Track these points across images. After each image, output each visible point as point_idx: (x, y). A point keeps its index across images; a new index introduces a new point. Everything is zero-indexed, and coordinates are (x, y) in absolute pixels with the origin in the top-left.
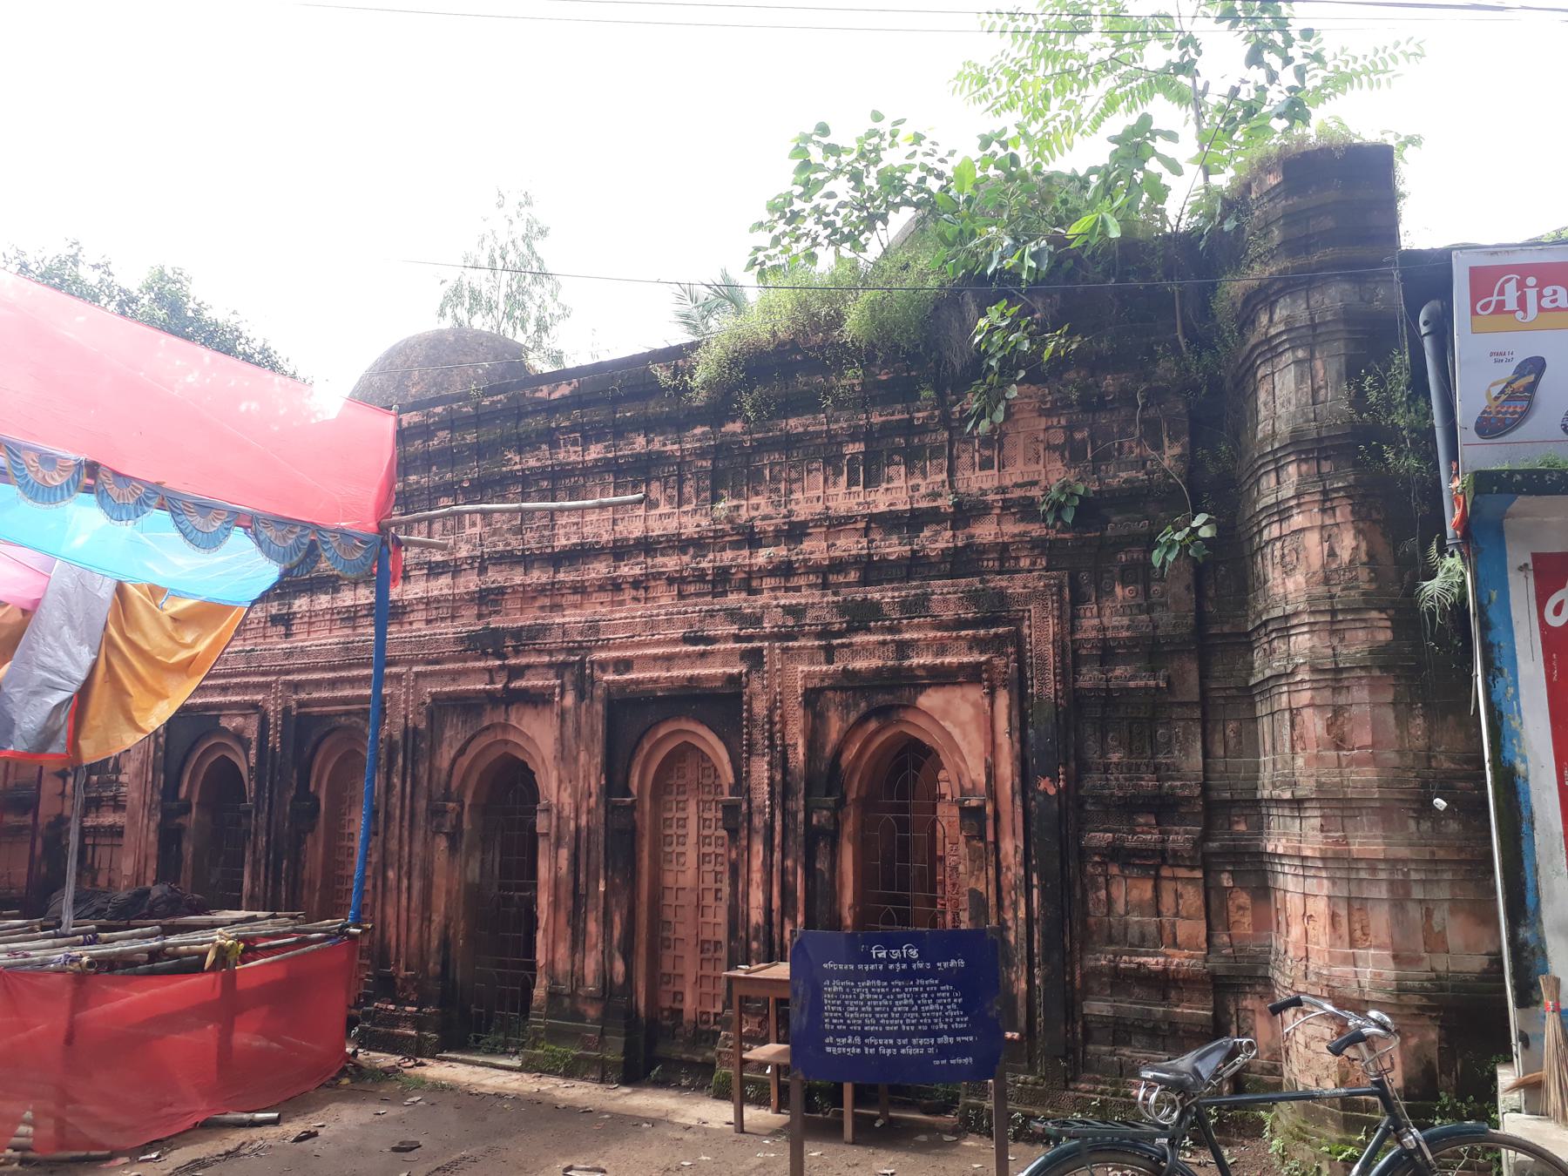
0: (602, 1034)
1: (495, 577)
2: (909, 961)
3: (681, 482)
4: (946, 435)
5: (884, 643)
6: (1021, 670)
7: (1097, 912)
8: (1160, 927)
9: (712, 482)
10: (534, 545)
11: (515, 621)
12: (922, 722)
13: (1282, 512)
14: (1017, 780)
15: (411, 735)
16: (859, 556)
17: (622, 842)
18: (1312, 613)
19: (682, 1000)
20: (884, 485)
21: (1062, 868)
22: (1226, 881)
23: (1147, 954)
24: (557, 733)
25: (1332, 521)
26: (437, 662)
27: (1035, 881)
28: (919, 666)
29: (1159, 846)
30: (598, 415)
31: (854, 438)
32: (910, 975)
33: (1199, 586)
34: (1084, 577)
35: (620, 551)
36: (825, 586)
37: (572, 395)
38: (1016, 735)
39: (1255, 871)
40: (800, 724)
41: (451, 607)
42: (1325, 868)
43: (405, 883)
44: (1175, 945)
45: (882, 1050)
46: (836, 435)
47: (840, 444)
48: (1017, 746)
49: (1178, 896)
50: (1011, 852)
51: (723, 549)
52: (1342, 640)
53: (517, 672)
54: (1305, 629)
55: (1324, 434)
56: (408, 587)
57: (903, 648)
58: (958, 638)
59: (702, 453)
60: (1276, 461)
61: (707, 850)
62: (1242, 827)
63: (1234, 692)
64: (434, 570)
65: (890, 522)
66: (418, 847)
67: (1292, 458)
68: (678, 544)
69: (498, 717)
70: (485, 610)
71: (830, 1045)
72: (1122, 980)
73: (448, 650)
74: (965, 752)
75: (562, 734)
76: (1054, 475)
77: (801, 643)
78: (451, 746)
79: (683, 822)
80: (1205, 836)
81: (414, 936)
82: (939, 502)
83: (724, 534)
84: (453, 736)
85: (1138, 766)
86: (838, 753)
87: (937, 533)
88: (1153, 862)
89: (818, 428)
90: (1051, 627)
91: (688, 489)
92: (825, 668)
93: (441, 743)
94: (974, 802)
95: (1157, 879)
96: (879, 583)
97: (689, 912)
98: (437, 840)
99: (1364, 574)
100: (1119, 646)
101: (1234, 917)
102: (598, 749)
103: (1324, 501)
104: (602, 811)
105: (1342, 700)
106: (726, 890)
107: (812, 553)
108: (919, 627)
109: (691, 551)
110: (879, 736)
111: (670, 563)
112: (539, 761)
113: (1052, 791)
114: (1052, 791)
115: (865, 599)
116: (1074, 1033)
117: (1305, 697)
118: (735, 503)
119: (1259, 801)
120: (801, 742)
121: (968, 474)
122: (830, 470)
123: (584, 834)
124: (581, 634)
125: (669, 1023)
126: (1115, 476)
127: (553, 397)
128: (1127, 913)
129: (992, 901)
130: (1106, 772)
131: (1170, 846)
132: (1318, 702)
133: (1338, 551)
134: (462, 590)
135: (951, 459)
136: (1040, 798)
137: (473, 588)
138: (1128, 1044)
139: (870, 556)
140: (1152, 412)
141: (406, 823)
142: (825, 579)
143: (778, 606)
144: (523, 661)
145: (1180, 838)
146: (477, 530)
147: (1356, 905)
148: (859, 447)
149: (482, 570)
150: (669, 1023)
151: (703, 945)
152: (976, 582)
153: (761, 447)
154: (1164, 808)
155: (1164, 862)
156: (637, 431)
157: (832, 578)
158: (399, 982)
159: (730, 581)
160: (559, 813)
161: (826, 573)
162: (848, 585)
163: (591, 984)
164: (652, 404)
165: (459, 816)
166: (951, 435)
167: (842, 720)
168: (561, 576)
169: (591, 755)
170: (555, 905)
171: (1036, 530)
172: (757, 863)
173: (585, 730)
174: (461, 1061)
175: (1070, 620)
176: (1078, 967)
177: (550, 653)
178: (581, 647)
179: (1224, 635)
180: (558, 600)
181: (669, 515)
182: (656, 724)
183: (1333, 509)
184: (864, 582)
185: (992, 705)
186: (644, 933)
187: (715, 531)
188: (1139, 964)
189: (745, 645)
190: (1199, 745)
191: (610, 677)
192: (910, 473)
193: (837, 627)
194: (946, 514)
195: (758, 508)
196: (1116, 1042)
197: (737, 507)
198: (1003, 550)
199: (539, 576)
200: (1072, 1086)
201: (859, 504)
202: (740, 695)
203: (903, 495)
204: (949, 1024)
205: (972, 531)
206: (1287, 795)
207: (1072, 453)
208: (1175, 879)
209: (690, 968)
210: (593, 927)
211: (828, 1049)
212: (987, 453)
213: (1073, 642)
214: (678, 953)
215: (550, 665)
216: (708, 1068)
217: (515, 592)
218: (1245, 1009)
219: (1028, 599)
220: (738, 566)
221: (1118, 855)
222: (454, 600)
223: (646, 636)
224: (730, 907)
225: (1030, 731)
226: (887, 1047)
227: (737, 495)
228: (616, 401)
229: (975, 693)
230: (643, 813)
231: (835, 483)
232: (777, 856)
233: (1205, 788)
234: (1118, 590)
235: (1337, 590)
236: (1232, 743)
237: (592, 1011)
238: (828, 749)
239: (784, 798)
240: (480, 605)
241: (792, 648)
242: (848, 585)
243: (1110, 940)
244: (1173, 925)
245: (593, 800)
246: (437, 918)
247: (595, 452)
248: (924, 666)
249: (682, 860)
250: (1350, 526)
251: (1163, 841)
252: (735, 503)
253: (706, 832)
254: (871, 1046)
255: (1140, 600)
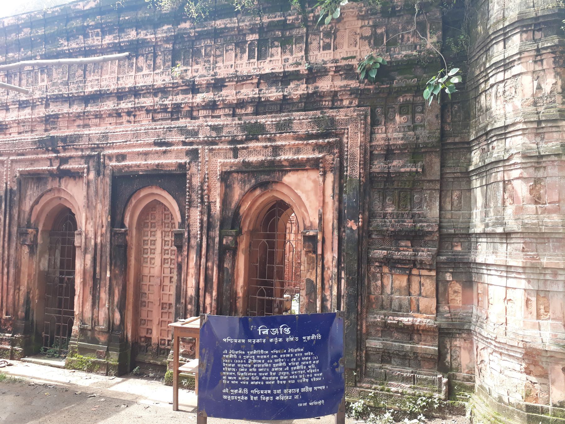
0: (108, 350)
1: (54, 109)
2: (284, 336)
3: (155, 56)
4: (305, 30)
5: (266, 147)
6: (341, 163)
7: (375, 292)
8: (410, 301)
9: (172, 58)
10: (74, 91)
11: (64, 132)
12: (285, 190)
13: (506, 65)
14: (336, 221)
15: (9, 193)
16: (254, 98)
17: (119, 251)
18: (525, 122)
19: (151, 333)
20: (269, 59)
21: (358, 269)
22: (449, 277)
23: (403, 316)
24: (85, 193)
25: (540, 68)
26: (23, 154)
27: (343, 275)
28: (285, 160)
29: (413, 258)
30: (110, 19)
31: (252, 31)
32: (283, 346)
33: (442, 116)
34: (379, 110)
35: (120, 95)
36: (234, 115)
37: (96, 7)
38: (337, 197)
39: (466, 272)
40: (218, 191)
41: (31, 125)
42: (524, 273)
43: (6, 270)
44: (418, 311)
45: (263, 398)
46: (242, 30)
47: (245, 35)
48: (337, 203)
49: (421, 284)
50: (330, 260)
51: (177, 94)
52: (542, 139)
53: (64, 160)
54: (520, 132)
55: (540, 14)
56: (8, 114)
57: (276, 150)
58: (308, 144)
59: (167, 40)
60: (505, 34)
61: (166, 256)
62: (459, 249)
63: (459, 175)
64: (22, 105)
65: (271, 79)
66: (12, 252)
67: (518, 30)
68: (155, 91)
69: (55, 184)
70: (49, 127)
71: (226, 394)
72: (387, 329)
73: (29, 148)
74: (307, 206)
75: (87, 193)
76: (365, 52)
77: (220, 146)
78: (30, 199)
79: (154, 242)
80: (439, 254)
81: (11, 297)
82: (300, 68)
83: (178, 85)
84: (32, 194)
85: (403, 215)
86: (238, 207)
87: (298, 86)
88: (408, 266)
89: (233, 25)
90: (359, 138)
91: (159, 61)
92: (232, 160)
93: (25, 197)
94: (311, 233)
95: (410, 275)
96: (264, 113)
97: (156, 288)
98: (23, 248)
99: (559, 99)
100: (396, 149)
101: (452, 296)
102: (107, 202)
103: (537, 56)
104: (108, 235)
105: (540, 174)
106: (175, 278)
107: (227, 96)
108: (285, 138)
109: (160, 95)
110: (262, 198)
111: (148, 102)
112: (77, 208)
113: (355, 228)
114: (355, 228)
115: (256, 122)
116: (361, 357)
117: (515, 173)
118: (185, 68)
119: (470, 234)
120: (218, 200)
121: (316, 53)
122: (238, 50)
123: (99, 247)
124: (98, 140)
125: (144, 344)
126: (398, 54)
127: (86, 8)
128: (392, 293)
129: (319, 285)
130: (384, 218)
131: (419, 258)
132: (525, 175)
133: (543, 86)
134: (36, 116)
135: (307, 44)
136: (348, 231)
137: (42, 115)
138: (389, 362)
139: (260, 98)
140: (421, 17)
141: (6, 239)
142: (234, 111)
143: (207, 126)
144: (68, 154)
145: (424, 254)
146: (43, 84)
147: (542, 294)
148: (256, 37)
149: (47, 106)
150: (144, 344)
151: (163, 306)
152: (318, 113)
153: (200, 36)
154: (416, 237)
155: (415, 266)
156: (131, 27)
157: (238, 111)
158: (2, 321)
159: (181, 112)
160: (86, 235)
161: (235, 108)
162: (247, 115)
163: (102, 325)
164: (140, 12)
165: (36, 236)
166: (307, 30)
167: (241, 189)
168: (89, 109)
169: (104, 206)
170: (84, 283)
171: (354, 84)
172: (192, 264)
173: (101, 192)
174: (34, 362)
175: (370, 134)
176: (364, 322)
177: (82, 150)
178: (98, 147)
179: (455, 143)
180: (87, 122)
181: (148, 75)
182: (139, 189)
183: (542, 61)
184: (256, 113)
185: (324, 181)
186: (132, 298)
187: (173, 84)
188: (398, 321)
189: (188, 147)
190: (438, 204)
191: (114, 163)
192: (283, 52)
193: (240, 138)
194: (303, 75)
195: (198, 72)
196: (383, 361)
197: (186, 71)
198: (334, 95)
199: (77, 109)
200: (358, 385)
201: (254, 69)
202: (185, 175)
203: (279, 64)
204: (310, 378)
205: (317, 84)
206: (500, 230)
207: (375, 40)
208: (420, 275)
209: (155, 317)
210: (104, 296)
211: (225, 397)
212: (327, 41)
213: (371, 146)
214: (149, 309)
215: (82, 157)
216: (163, 368)
217: (64, 117)
218: (456, 346)
219: (347, 122)
220: (185, 103)
221: (389, 262)
222: (32, 122)
223: (135, 142)
224: (177, 287)
225: (344, 195)
226: (266, 395)
227: (186, 64)
228: (120, 11)
229: (315, 175)
230: (132, 237)
231: (241, 58)
232: (203, 260)
233: (440, 227)
234: (397, 118)
235: (542, 109)
236: (455, 203)
237: (103, 338)
238: (233, 205)
239: (209, 230)
240: (46, 125)
241: (215, 150)
242: (247, 115)
243: (382, 307)
244: (418, 300)
245: (104, 229)
246: (23, 288)
247: (108, 39)
248: (287, 160)
249: (153, 262)
250: (552, 71)
251: (415, 255)
252: (185, 68)
253: (166, 248)
254: (255, 395)
255: (410, 124)
